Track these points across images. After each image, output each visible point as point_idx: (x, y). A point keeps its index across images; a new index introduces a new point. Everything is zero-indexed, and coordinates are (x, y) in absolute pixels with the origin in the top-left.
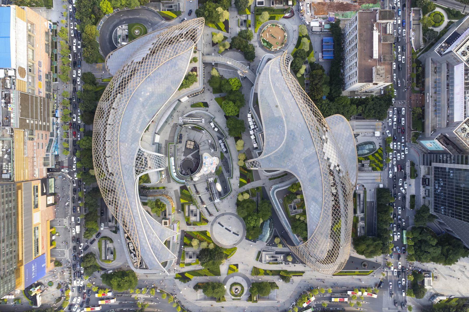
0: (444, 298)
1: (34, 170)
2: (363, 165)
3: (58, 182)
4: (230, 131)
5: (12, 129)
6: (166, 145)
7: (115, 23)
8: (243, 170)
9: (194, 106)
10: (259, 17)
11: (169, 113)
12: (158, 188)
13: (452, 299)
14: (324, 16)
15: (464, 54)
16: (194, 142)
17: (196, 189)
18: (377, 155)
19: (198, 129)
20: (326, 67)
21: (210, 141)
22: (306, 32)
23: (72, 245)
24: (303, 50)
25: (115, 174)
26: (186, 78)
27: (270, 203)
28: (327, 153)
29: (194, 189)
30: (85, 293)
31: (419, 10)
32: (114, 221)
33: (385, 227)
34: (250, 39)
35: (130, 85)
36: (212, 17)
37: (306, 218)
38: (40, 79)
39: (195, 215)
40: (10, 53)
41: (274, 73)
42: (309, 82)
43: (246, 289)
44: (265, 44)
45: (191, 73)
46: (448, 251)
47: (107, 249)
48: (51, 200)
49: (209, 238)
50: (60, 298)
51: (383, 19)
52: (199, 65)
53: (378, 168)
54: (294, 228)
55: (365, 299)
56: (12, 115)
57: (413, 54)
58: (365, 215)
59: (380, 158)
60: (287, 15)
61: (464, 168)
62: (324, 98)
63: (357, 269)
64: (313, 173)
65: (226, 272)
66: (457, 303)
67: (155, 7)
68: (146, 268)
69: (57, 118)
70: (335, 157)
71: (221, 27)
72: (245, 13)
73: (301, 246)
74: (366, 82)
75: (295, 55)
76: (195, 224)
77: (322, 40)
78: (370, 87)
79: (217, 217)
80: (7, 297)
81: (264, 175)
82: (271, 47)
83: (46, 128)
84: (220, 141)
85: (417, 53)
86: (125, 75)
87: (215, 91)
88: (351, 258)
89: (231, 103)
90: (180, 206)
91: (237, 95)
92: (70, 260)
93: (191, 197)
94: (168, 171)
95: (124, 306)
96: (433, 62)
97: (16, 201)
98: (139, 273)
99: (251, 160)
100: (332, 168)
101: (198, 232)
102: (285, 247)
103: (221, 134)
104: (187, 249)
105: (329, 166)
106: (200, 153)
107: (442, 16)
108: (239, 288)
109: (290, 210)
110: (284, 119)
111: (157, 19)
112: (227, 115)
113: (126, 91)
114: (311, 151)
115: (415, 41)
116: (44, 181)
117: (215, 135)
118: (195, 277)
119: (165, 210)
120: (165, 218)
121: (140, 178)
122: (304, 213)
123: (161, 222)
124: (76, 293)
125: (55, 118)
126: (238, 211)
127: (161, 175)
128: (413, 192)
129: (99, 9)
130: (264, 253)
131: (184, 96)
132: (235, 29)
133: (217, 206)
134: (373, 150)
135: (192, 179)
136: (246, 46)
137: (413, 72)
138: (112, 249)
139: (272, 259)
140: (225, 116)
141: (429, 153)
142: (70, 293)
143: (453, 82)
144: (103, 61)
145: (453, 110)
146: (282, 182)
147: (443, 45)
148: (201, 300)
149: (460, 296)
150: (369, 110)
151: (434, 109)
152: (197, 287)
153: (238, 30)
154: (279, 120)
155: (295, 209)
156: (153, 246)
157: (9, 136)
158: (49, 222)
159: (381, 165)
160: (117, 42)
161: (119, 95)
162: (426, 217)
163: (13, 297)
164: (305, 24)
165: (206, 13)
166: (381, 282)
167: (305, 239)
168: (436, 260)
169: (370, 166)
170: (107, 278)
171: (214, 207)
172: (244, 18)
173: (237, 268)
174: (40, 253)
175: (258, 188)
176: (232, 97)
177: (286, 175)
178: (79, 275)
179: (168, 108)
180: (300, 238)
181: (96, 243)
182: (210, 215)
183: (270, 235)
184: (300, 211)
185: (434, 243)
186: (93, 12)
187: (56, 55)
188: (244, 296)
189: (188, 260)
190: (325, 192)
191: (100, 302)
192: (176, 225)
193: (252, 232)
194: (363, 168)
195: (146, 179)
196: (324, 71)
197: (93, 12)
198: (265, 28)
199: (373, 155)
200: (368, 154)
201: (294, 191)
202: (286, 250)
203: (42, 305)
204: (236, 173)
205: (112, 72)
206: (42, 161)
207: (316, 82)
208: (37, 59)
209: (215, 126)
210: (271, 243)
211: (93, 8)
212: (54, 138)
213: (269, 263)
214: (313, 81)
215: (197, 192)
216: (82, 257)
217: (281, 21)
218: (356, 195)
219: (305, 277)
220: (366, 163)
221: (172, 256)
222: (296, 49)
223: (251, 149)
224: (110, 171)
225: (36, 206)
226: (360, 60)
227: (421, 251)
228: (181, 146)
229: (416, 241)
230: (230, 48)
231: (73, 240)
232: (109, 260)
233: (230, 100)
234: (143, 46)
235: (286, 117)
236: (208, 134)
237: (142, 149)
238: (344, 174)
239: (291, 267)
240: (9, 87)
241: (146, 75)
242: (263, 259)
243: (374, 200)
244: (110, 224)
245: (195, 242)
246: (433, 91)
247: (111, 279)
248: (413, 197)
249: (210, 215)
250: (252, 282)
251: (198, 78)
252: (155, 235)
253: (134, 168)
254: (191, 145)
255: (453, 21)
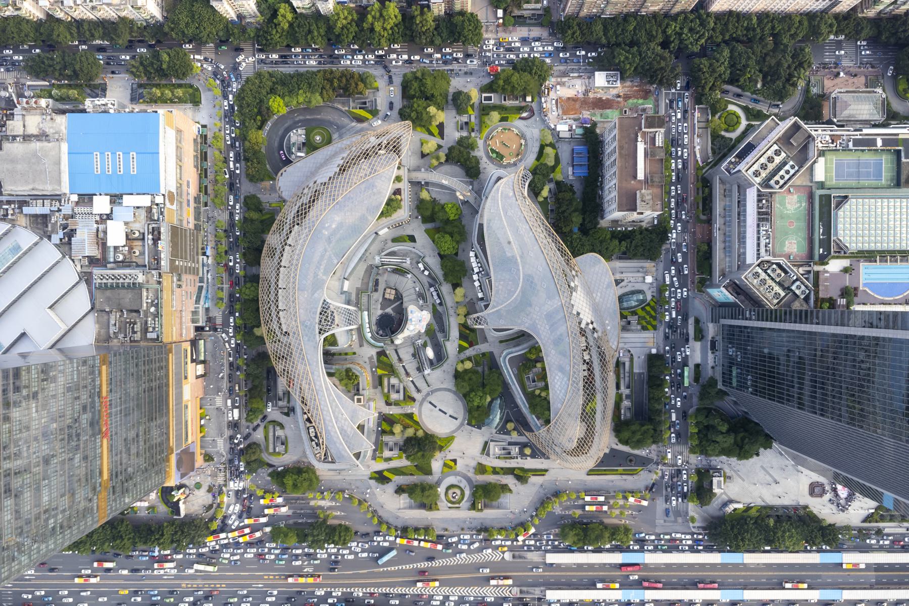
0: (740, 506)
1: (181, 329)
2: (629, 323)
3: (209, 345)
4: (446, 276)
5: (160, 274)
6: (357, 295)
7: (286, 125)
8: (464, 329)
9: (395, 240)
10: (486, 119)
11: (362, 251)
12: (346, 354)
13: (752, 507)
14: (575, 116)
15: (756, 174)
16: (396, 289)
17: (398, 356)
18: (648, 308)
19: (400, 271)
20: (577, 187)
21: (417, 289)
22: (549, 139)
23: (227, 433)
24: (545, 164)
25: (291, 334)
26: (388, 204)
27: (501, 374)
28: (576, 305)
29: (396, 356)
30: (245, 499)
31: (707, 109)
32: (286, 400)
33: (657, 407)
34: (473, 149)
35: (312, 213)
36: (422, 120)
37: (548, 394)
38: (188, 205)
39: (398, 392)
40: (158, 173)
41: (505, 197)
42: (554, 208)
43: (467, 493)
44: (494, 155)
45: (393, 197)
46: (743, 439)
47: (277, 438)
48: (200, 369)
49: (417, 423)
50: (211, 506)
51: (649, 127)
52: (404, 186)
53: (649, 327)
54: (533, 407)
55: (631, 507)
56: (163, 256)
57: (698, 169)
58: (631, 391)
59: (653, 313)
60: (524, 115)
61: (768, 326)
62: (576, 230)
63: (620, 465)
64: (558, 333)
65: (440, 470)
66: (758, 514)
67: (343, 104)
68: (333, 462)
69: (208, 257)
70: (587, 310)
71: (433, 131)
72: (467, 112)
73: (543, 431)
74: (628, 210)
75: (534, 171)
76: (397, 403)
77: (573, 150)
78: (634, 216)
79: (428, 395)
80: (138, 504)
81: (492, 335)
82: (502, 159)
83: (195, 271)
84: (432, 289)
85: (703, 168)
86: (305, 200)
87: (425, 220)
88: (612, 450)
89: (448, 237)
90: (377, 378)
91: (456, 226)
92: (224, 454)
93: (391, 366)
94: (360, 330)
95: (300, 516)
96: (722, 182)
97: (167, 367)
98: (322, 469)
99: (475, 315)
100: (583, 326)
101: (401, 414)
102: (521, 435)
103: (434, 279)
104: (386, 438)
105: (580, 323)
106: (405, 305)
107: (738, 117)
108: (458, 492)
109: (528, 383)
110: (519, 260)
111: (345, 120)
112: (442, 253)
113: (306, 222)
114: (556, 303)
115: (701, 151)
116: (194, 343)
117: (425, 281)
118: (397, 477)
119: (358, 383)
120: (359, 394)
121: (325, 340)
122: (546, 388)
123: (353, 400)
124: (233, 498)
125: (205, 257)
126: (457, 385)
127: (352, 335)
128: (698, 359)
129: (268, 109)
130: (492, 444)
131: (383, 228)
132: (453, 135)
133: (428, 378)
134: (643, 301)
135: (392, 342)
136: (468, 158)
137: (698, 193)
138: (283, 437)
139: (503, 452)
140: (439, 254)
141: (720, 306)
142: (225, 499)
143: (745, 211)
144: (274, 179)
145: (745, 248)
146: (518, 345)
147: (733, 160)
148: (405, 508)
149: (763, 504)
150: (636, 246)
151: (723, 246)
152: (400, 490)
153: (457, 135)
154: (512, 260)
155: (534, 381)
156: (342, 431)
157: (155, 282)
158: (198, 400)
159: (654, 323)
160: (290, 153)
161: (296, 226)
162: (713, 393)
163: (146, 504)
164: (549, 128)
165: (413, 115)
166: (654, 484)
167: (548, 422)
168: (728, 452)
169: (638, 323)
170: (279, 476)
171: (423, 380)
172: (465, 118)
173: (456, 464)
174: (190, 441)
175: (484, 354)
176: (449, 228)
177: (522, 336)
178: (237, 474)
179: (361, 244)
180: (541, 421)
181: (261, 430)
182: (419, 391)
183: (501, 419)
184: (541, 384)
185: (724, 428)
186: (260, 113)
187: (206, 170)
188: (465, 504)
189: (387, 454)
190: (574, 357)
191: (267, 511)
192: (372, 404)
193: (476, 414)
194: (629, 327)
195: (331, 341)
196: (574, 193)
197: (260, 113)
198: (494, 133)
199: (643, 309)
200: (635, 307)
201: (533, 357)
202: (523, 439)
203: (186, 516)
204: (454, 333)
205: (285, 195)
206: (190, 316)
207: (563, 209)
208: (186, 177)
209: (425, 269)
210: (503, 430)
211: (260, 108)
212: (205, 285)
213: (499, 458)
214: (559, 208)
215: (400, 360)
216: (241, 450)
217: (517, 124)
218: (619, 364)
219: (548, 477)
220: (634, 320)
221: (367, 446)
222: (537, 163)
223: (475, 300)
224: (284, 330)
225: (186, 378)
226: (620, 181)
227: (708, 441)
228: (377, 296)
229: (701, 427)
230: (447, 161)
231: (229, 427)
232: (279, 453)
233: (446, 233)
234: (327, 162)
235: (521, 257)
236: (415, 279)
237: (328, 300)
238: (600, 334)
239: (530, 463)
240: (156, 218)
241: (334, 200)
242: (491, 452)
243: (645, 371)
244: (280, 403)
245: (397, 429)
246: (722, 221)
247: (284, 477)
248: (697, 366)
249: (419, 391)
250: (475, 484)
251: (402, 203)
252: (345, 416)
253: (317, 326)
254: (390, 294)
255: (753, 123)
